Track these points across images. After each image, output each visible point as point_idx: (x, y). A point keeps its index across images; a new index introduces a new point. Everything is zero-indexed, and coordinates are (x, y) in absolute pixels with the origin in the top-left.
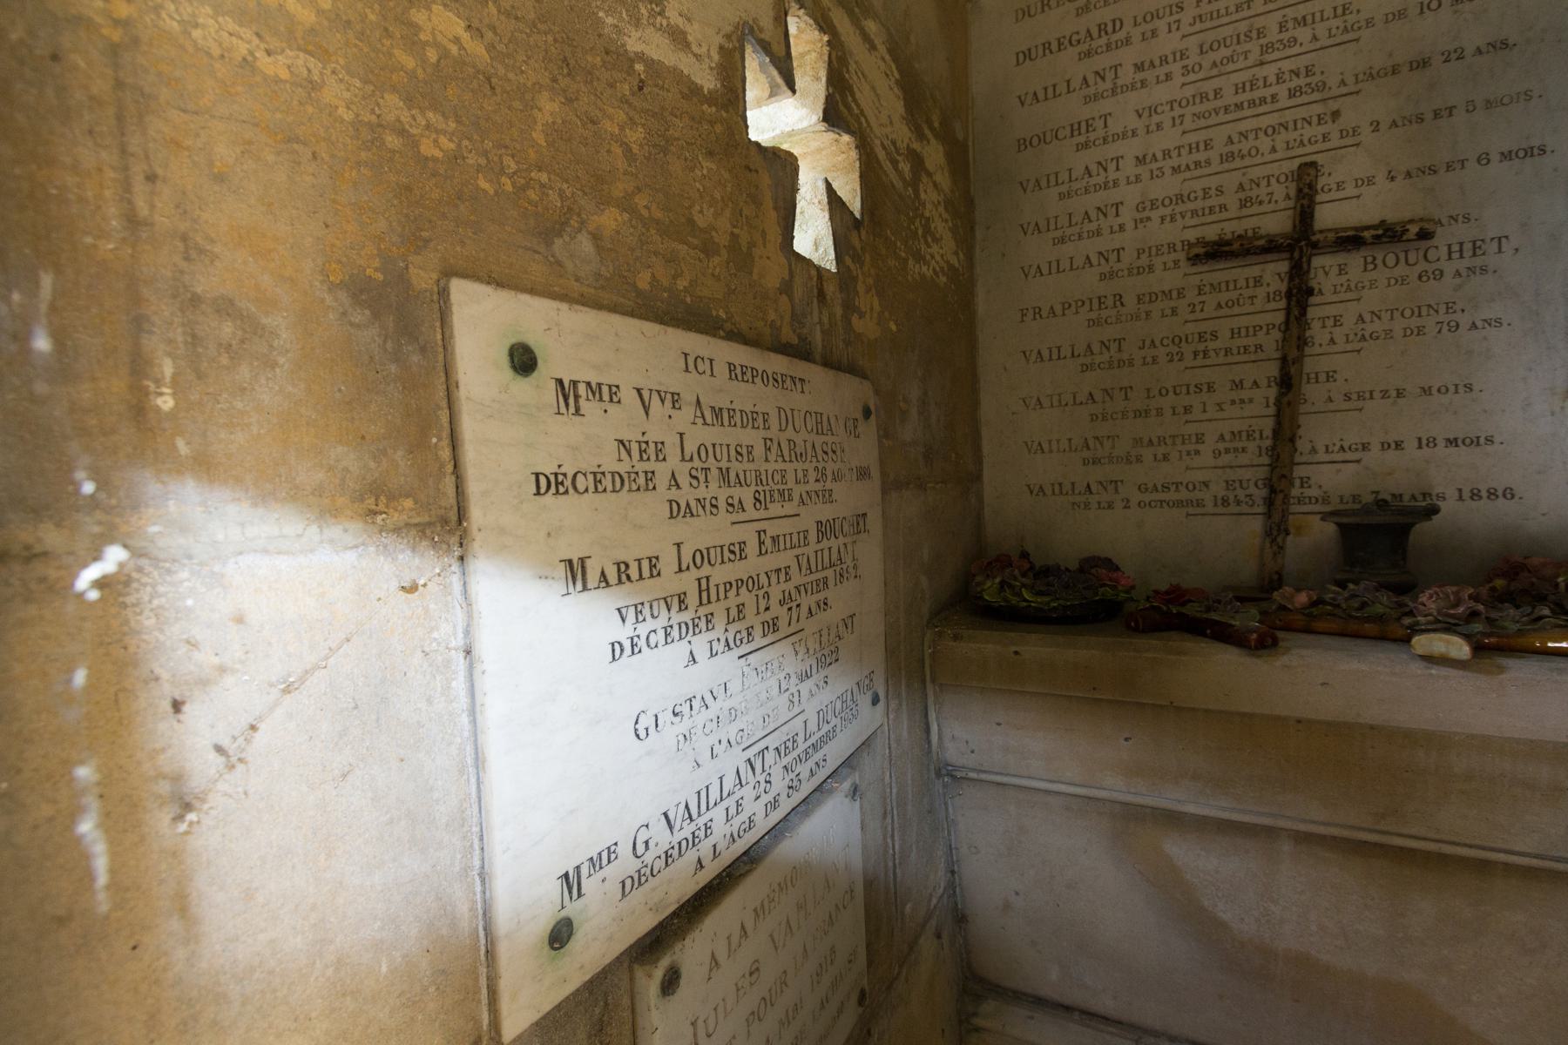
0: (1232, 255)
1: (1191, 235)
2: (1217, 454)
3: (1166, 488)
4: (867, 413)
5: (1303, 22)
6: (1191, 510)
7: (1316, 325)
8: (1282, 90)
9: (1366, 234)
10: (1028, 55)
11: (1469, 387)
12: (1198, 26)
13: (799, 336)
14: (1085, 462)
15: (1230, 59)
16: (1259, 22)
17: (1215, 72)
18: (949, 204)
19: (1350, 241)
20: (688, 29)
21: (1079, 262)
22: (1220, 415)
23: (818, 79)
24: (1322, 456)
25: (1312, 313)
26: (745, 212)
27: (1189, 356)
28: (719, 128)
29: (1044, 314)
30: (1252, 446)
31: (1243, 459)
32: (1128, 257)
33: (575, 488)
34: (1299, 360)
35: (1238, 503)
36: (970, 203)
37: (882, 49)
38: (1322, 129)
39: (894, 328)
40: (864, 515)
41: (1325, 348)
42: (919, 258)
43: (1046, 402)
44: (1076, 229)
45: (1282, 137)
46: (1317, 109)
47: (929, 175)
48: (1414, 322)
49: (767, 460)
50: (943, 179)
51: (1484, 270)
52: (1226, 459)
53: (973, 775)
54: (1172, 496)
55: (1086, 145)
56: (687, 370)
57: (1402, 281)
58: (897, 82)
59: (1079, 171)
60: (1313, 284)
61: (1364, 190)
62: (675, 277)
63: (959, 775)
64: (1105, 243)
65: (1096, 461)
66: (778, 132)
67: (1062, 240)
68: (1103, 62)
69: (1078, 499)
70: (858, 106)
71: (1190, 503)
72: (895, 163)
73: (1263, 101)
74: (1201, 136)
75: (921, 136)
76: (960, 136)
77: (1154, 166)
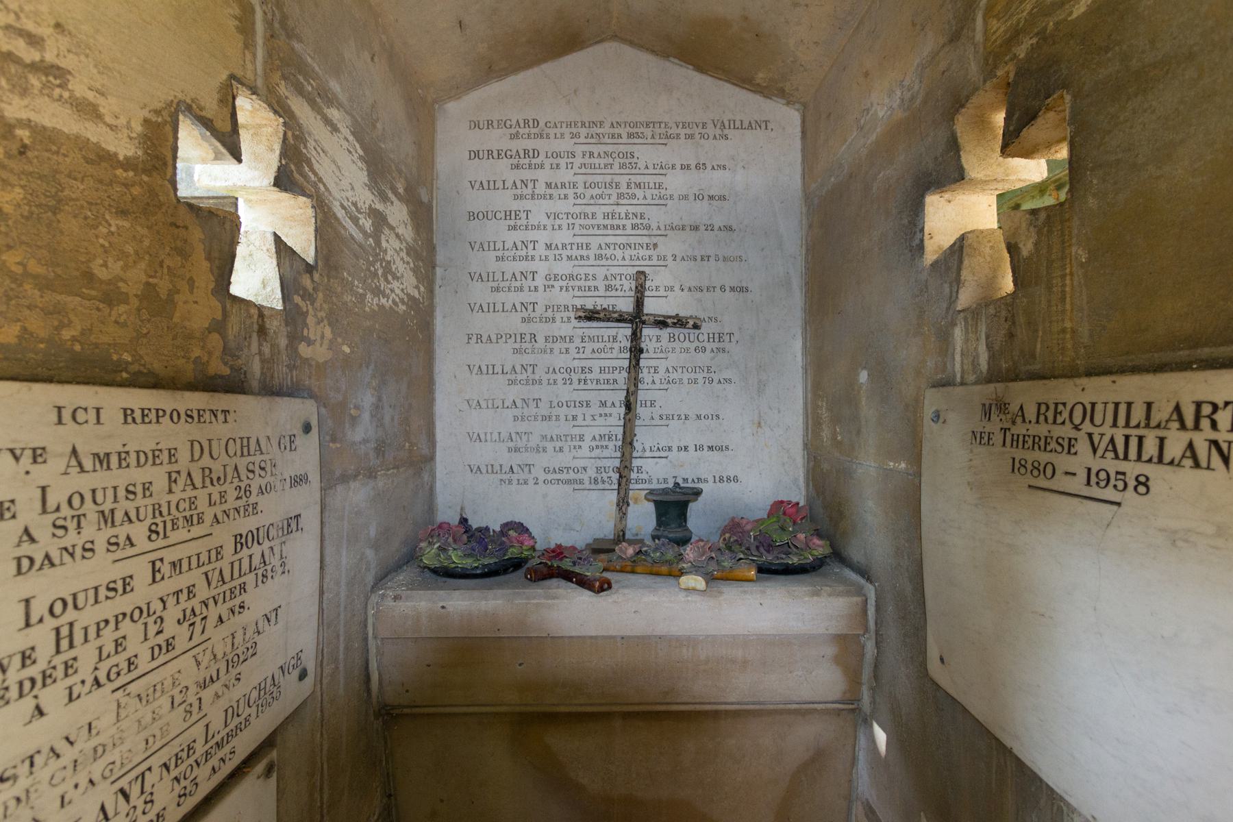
0: (599, 319)
1: (578, 303)
2: (592, 449)
3: (561, 470)
4: (307, 428)
5: (638, 186)
6: (576, 487)
7: (646, 371)
8: (628, 223)
9: (669, 321)
10: (477, 154)
11: (718, 416)
12: (583, 170)
13: (231, 368)
14: (510, 450)
15: (601, 196)
16: (617, 179)
17: (592, 202)
18: (410, 251)
19: (661, 323)
20: (100, 101)
21: (508, 307)
22: (592, 423)
23: (272, 150)
24: (648, 454)
25: (642, 363)
26: (168, 262)
27: (575, 381)
28: (136, 191)
29: (484, 339)
30: (611, 445)
31: (606, 453)
32: (540, 309)
34: (635, 393)
35: (603, 482)
36: (432, 249)
37: (346, 132)
38: (649, 253)
39: (347, 349)
40: (298, 516)
41: (650, 386)
42: (378, 292)
43: (483, 404)
44: (507, 284)
45: (628, 252)
46: (646, 240)
47: (392, 228)
48: (693, 376)
49: (170, 491)
50: (407, 233)
51: (724, 351)
52: (597, 452)
53: (406, 711)
54: (564, 476)
55: (514, 228)
56: (60, 422)
57: (687, 350)
58: (360, 157)
59: (509, 245)
60: (643, 345)
61: (669, 293)
62: (58, 329)
64: (526, 297)
65: (517, 450)
66: (230, 183)
67: (497, 289)
68: (527, 174)
69: (505, 477)
70: (316, 174)
71: (575, 481)
72: (355, 220)
73: (618, 227)
74: (584, 240)
75: (384, 198)
76: (425, 199)
77: (557, 252)
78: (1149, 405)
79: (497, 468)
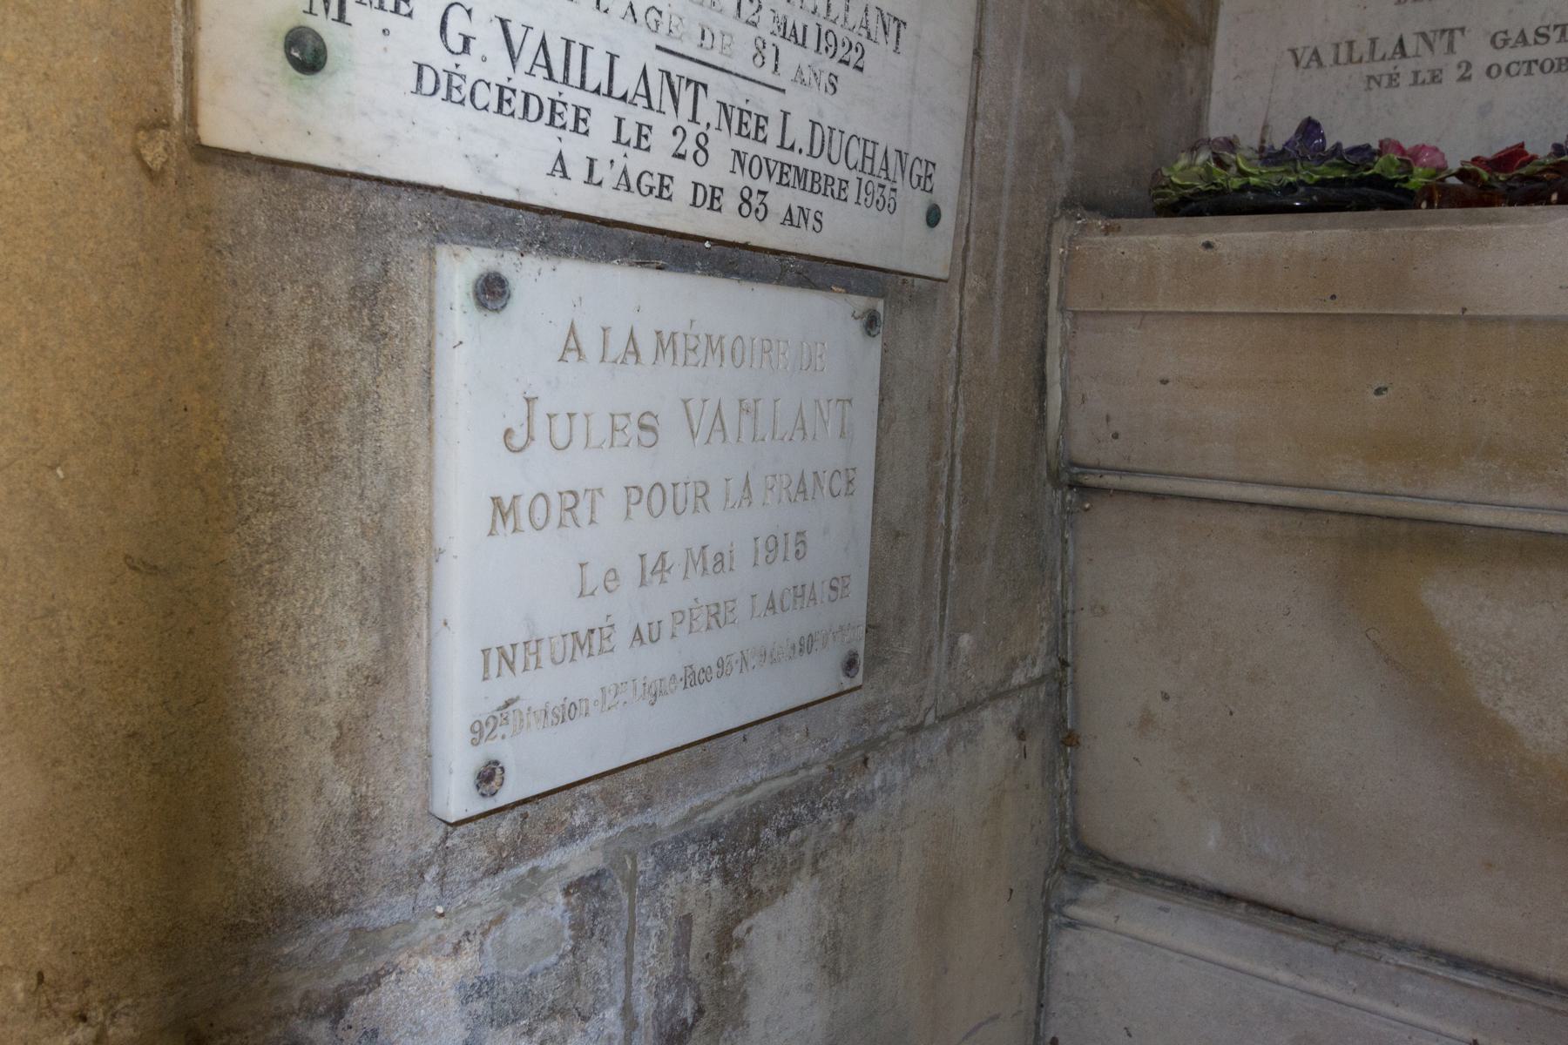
33: (472, 101)
53: (1112, 480)
63: (1091, 480)
69: (1380, 68)
78: (1373, 41)
79: (1362, 47)
